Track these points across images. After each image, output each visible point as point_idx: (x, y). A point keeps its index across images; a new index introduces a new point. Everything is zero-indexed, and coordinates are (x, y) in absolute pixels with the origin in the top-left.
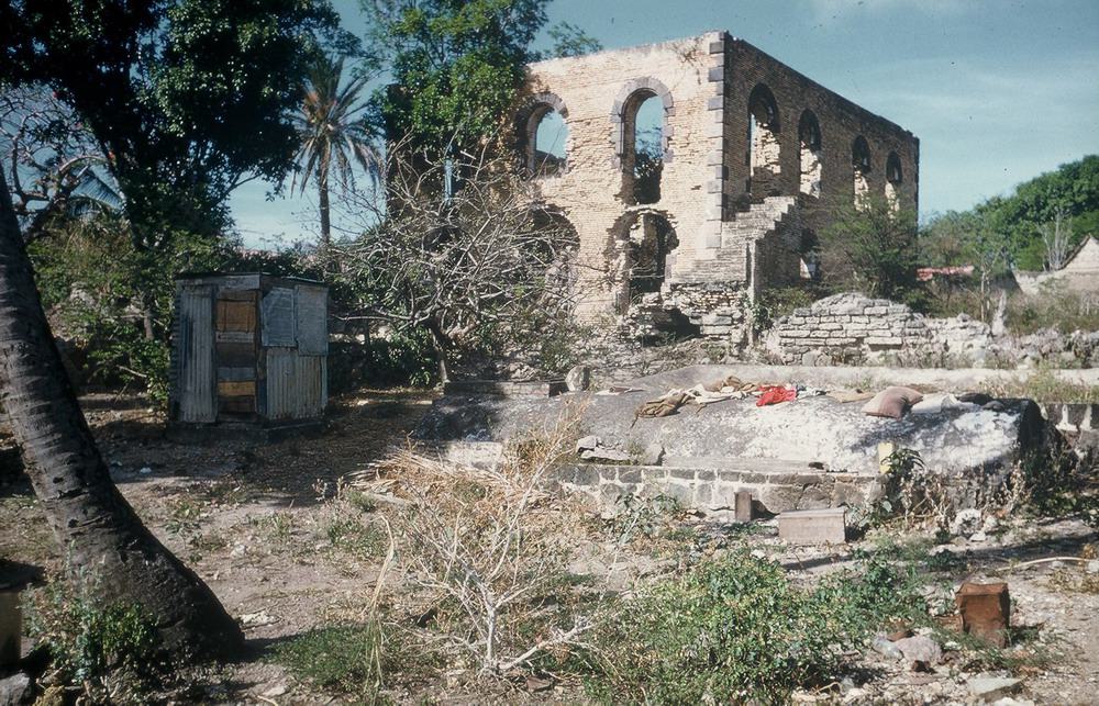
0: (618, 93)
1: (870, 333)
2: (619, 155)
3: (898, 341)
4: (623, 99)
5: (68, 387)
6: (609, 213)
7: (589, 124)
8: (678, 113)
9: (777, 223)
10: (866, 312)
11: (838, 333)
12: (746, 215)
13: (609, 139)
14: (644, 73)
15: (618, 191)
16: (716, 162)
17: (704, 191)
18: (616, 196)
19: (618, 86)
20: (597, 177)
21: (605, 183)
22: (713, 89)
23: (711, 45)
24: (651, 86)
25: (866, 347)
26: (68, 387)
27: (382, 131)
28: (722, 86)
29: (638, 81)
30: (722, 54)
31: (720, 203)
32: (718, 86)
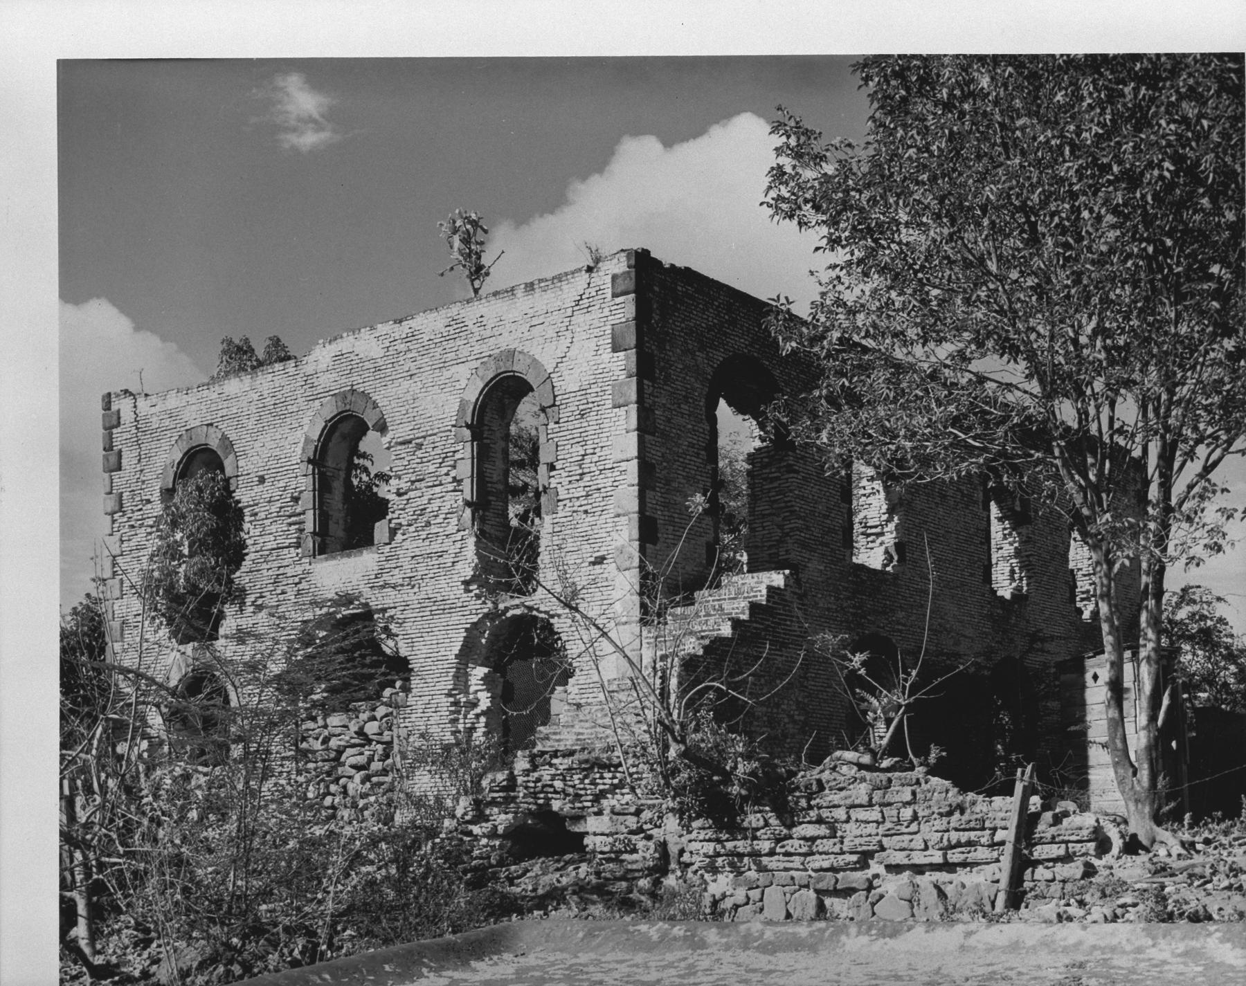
0: (465, 386)
1: (885, 841)
2: (468, 504)
3: (937, 858)
4: (472, 395)
5: (95, 899)
6: (455, 618)
7: (419, 446)
8: (564, 415)
9: (736, 623)
10: (876, 799)
11: (827, 845)
12: (690, 610)
13: (453, 473)
14: (506, 341)
15: (468, 573)
16: (629, 456)
17: (610, 568)
18: (466, 583)
19: (463, 372)
20: (436, 547)
21: (448, 559)
22: (620, 365)
23: (614, 278)
24: (520, 367)
25: (881, 870)
26: (95, 899)
27: (767, 808)
28: (634, 358)
29: (497, 359)
30: (636, 488)
31: (633, 368)
32: (627, 358)
